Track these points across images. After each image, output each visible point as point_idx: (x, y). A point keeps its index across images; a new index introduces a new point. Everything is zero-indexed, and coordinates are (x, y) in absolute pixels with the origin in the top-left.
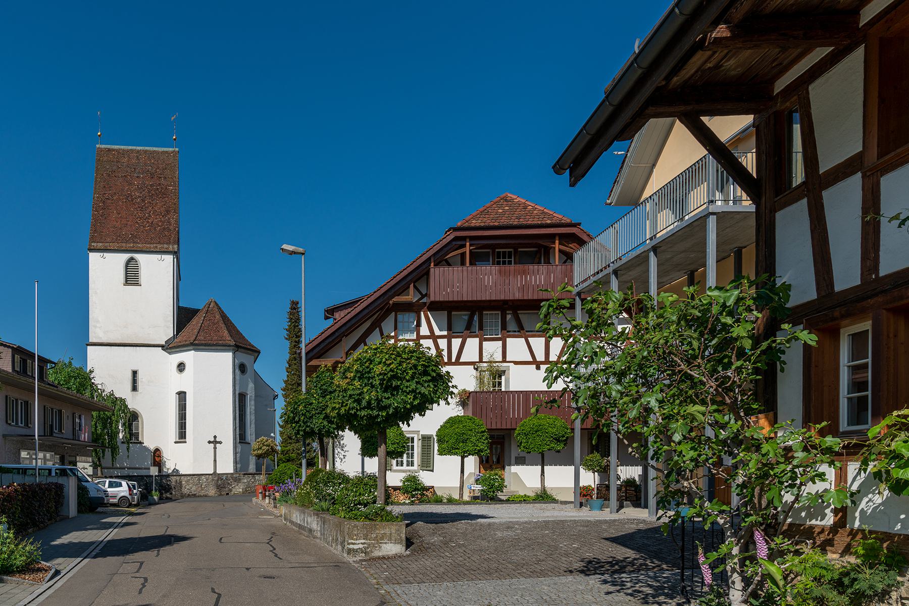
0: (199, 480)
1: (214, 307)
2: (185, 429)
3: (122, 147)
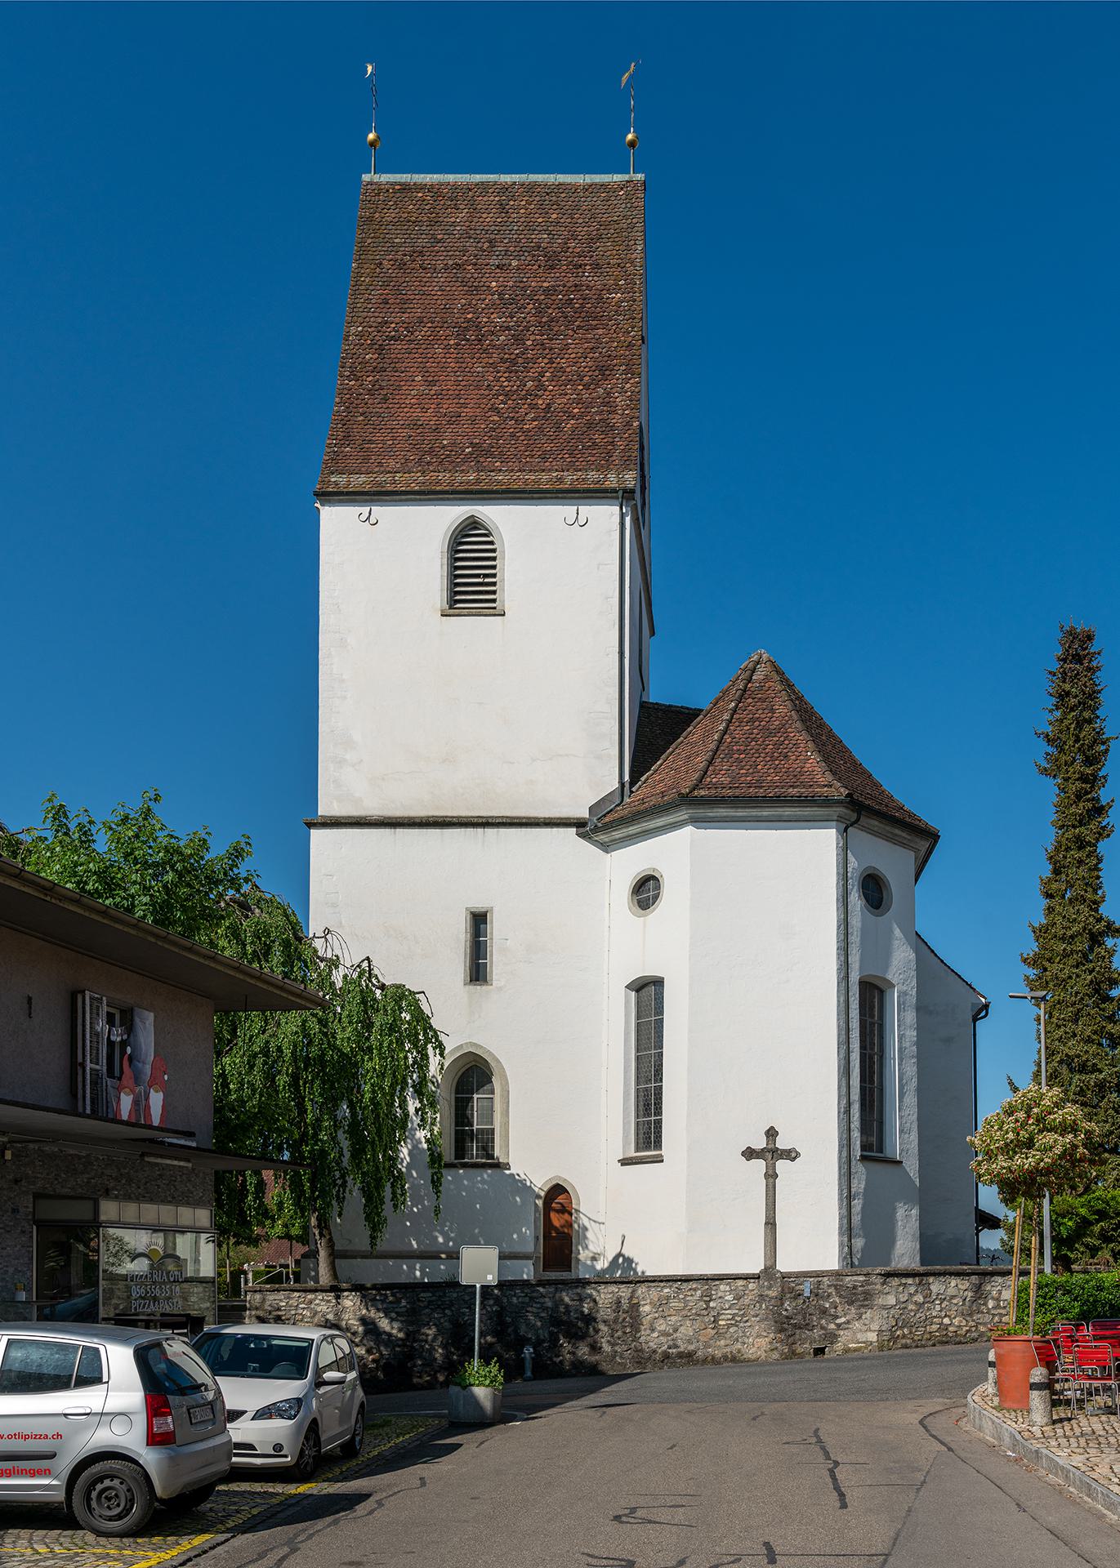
0: (708, 1297)
1: (767, 678)
2: (659, 1111)
3: (451, 178)
